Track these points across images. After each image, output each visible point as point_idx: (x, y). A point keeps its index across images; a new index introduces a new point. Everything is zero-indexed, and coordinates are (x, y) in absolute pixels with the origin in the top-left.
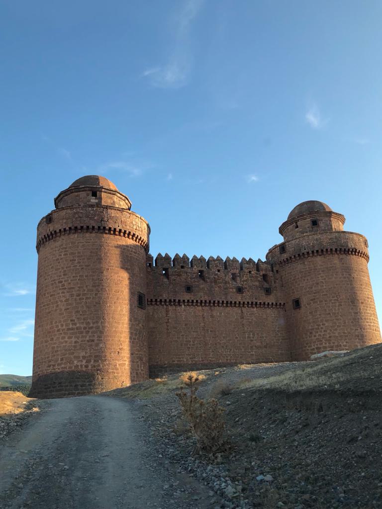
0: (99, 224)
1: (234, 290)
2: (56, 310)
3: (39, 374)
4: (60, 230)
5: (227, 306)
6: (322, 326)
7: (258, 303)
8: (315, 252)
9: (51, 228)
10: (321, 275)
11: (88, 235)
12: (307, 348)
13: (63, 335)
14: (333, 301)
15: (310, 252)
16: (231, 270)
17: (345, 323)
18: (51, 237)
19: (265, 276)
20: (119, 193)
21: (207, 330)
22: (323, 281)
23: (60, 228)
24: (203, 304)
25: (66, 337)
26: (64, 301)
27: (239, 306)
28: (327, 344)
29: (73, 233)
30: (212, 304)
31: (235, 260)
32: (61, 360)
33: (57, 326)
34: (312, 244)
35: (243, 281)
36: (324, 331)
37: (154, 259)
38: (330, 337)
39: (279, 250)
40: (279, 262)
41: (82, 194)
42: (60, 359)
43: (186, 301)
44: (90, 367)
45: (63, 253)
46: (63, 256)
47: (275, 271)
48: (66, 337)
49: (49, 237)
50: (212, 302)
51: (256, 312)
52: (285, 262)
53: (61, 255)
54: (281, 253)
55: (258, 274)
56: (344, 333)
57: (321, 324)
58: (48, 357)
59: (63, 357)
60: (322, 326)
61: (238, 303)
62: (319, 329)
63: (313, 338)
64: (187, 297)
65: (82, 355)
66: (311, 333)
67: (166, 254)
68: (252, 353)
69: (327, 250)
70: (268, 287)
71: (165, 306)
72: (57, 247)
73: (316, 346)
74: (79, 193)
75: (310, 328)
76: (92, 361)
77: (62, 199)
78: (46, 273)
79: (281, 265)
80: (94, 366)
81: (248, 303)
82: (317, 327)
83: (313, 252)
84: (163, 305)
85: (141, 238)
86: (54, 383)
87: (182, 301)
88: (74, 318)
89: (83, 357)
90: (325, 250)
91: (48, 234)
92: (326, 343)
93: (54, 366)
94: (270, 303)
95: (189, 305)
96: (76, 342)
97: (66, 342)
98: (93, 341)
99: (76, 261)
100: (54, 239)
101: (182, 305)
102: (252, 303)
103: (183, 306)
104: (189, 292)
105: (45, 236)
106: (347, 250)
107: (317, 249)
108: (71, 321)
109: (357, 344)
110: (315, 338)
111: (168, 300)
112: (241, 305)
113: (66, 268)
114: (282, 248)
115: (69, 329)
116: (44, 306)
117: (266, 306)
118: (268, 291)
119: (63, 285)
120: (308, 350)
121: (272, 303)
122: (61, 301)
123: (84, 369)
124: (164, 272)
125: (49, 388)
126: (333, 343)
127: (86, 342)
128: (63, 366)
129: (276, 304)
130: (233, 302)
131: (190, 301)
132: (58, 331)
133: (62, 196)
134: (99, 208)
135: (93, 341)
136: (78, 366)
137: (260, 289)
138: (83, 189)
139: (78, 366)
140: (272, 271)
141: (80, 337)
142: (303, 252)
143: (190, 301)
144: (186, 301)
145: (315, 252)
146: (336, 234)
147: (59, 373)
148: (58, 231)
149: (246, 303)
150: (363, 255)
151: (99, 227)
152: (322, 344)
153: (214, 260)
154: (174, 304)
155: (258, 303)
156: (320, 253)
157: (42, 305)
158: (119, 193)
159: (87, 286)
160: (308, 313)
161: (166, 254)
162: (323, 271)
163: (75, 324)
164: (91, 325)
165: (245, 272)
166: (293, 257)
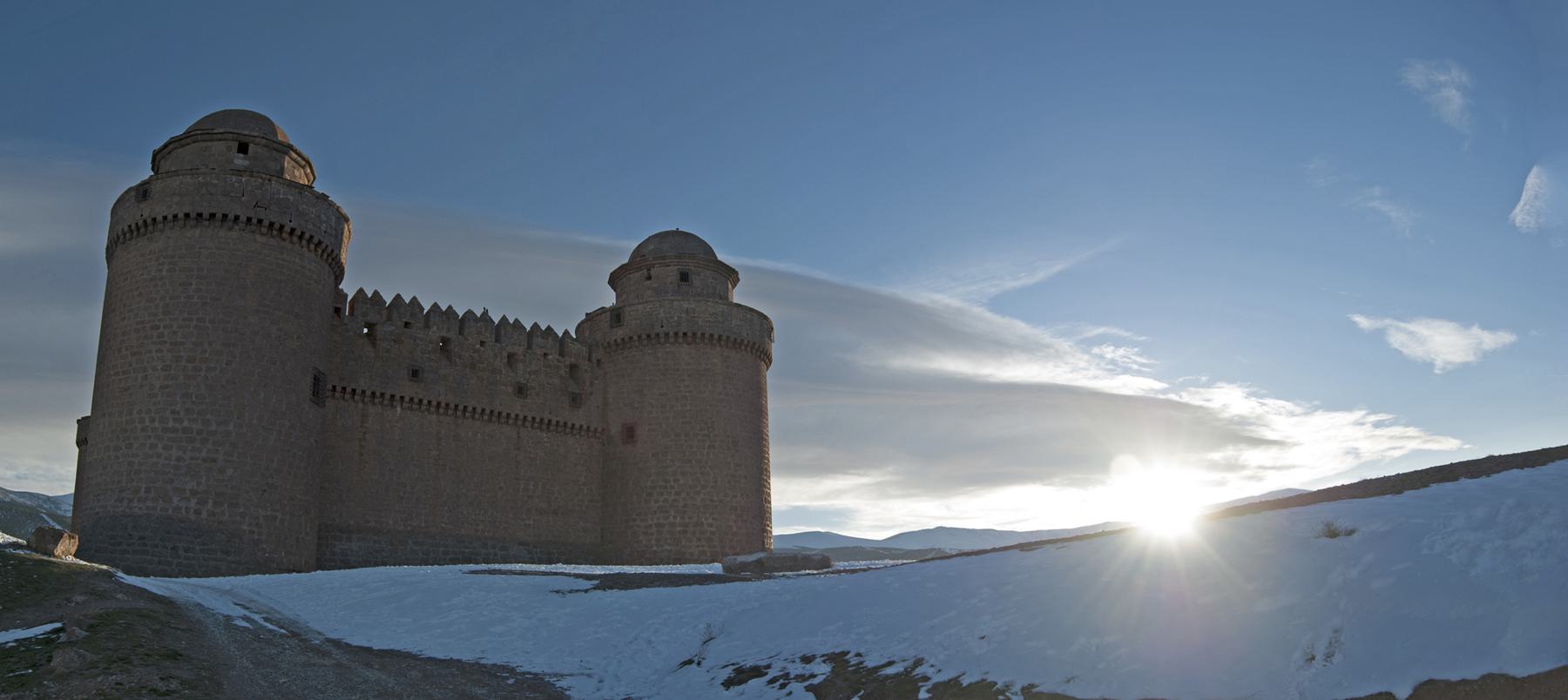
0: (251, 214)
1: (510, 389)
2: (141, 386)
3: (98, 513)
4: (165, 218)
5: (490, 420)
6: (672, 483)
7: (554, 423)
8: (681, 334)
9: (147, 210)
10: (686, 383)
11: (222, 233)
12: (638, 522)
13: (153, 440)
14: (699, 437)
15: (671, 334)
16: (507, 346)
17: (716, 482)
18: (142, 230)
19: (573, 368)
20: (296, 152)
21: (443, 465)
22: (687, 394)
23: (165, 214)
24: (441, 411)
25: (160, 446)
26: (159, 368)
27: (515, 424)
28: (678, 518)
29: (192, 227)
30: (459, 413)
31: (517, 324)
32: (145, 492)
33: (142, 421)
34: (676, 318)
35: (529, 373)
36: (676, 494)
37: (349, 299)
38: (685, 506)
39: (608, 319)
40: (606, 344)
41: (218, 147)
42: (143, 490)
43: (407, 399)
44: (204, 515)
45: (166, 267)
46: (164, 273)
47: (594, 361)
48: (160, 446)
49: (138, 228)
50: (461, 407)
51: (546, 440)
52: (617, 345)
53: (161, 270)
54: (612, 327)
55: (560, 362)
56: (712, 501)
57: (672, 479)
58: (119, 482)
59: (151, 485)
60: (672, 483)
61: (513, 416)
62: (666, 487)
63: (652, 503)
64: (409, 389)
65: (191, 488)
66: (650, 495)
67: (376, 293)
68: (527, 522)
69: (703, 334)
70: (577, 391)
71: (361, 405)
72: (155, 253)
73: (655, 521)
74: (210, 143)
75: (649, 484)
76: (211, 502)
77: (170, 153)
78: (125, 305)
79: (608, 350)
80: (214, 514)
81: (534, 418)
82: (663, 483)
83: (676, 334)
84: (357, 402)
85: (333, 251)
86: (130, 535)
87: (398, 397)
88: (178, 408)
89: (190, 490)
90: (699, 334)
91: (137, 224)
92: (675, 517)
93: (130, 501)
94: (577, 426)
95: (411, 409)
96: (179, 459)
97: (159, 456)
98: (214, 461)
99: (193, 287)
100: (149, 235)
101: (396, 407)
102: (542, 420)
103: (399, 409)
104: (415, 381)
105: (130, 226)
106: (739, 341)
107: (685, 331)
108: (173, 412)
109: (731, 523)
110: (657, 505)
111: (368, 393)
112: (520, 423)
113: (171, 299)
114: (616, 315)
115: (166, 430)
116: (117, 374)
117: (568, 430)
118: (576, 400)
119: (161, 335)
120: (638, 526)
121: (581, 426)
122: (154, 369)
123: (192, 517)
124: (366, 330)
125: (120, 543)
126: (690, 518)
127: (200, 461)
128: (149, 504)
129: (588, 427)
130: (504, 414)
131: (416, 400)
132: (143, 429)
133: (171, 147)
134: (253, 179)
135: (214, 461)
136: (180, 509)
137: (560, 393)
138: (219, 136)
139: (180, 509)
140: (589, 360)
141: (190, 448)
142: (658, 331)
143: (416, 400)
144: (407, 399)
145: (681, 334)
146: (725, 307)
147: (140, 516)
148: (159, 218)
149: (530, 419)
150: (761, 352)
151: (249, 220)
152: (668, 517)
153: (477, 320)
154: (381, 403)
155: (554, 423)
156: (690, 339)
157: (112, 372)
158: (296, 152)
159: (210, 344)
160: (650, 455)
161: (376, 293)
162: (689, 376)
163: (181, 421)
164: (213, 428)
165: (535, 353)
166: (635, 338)
